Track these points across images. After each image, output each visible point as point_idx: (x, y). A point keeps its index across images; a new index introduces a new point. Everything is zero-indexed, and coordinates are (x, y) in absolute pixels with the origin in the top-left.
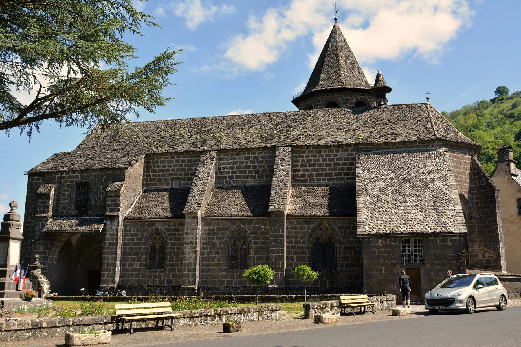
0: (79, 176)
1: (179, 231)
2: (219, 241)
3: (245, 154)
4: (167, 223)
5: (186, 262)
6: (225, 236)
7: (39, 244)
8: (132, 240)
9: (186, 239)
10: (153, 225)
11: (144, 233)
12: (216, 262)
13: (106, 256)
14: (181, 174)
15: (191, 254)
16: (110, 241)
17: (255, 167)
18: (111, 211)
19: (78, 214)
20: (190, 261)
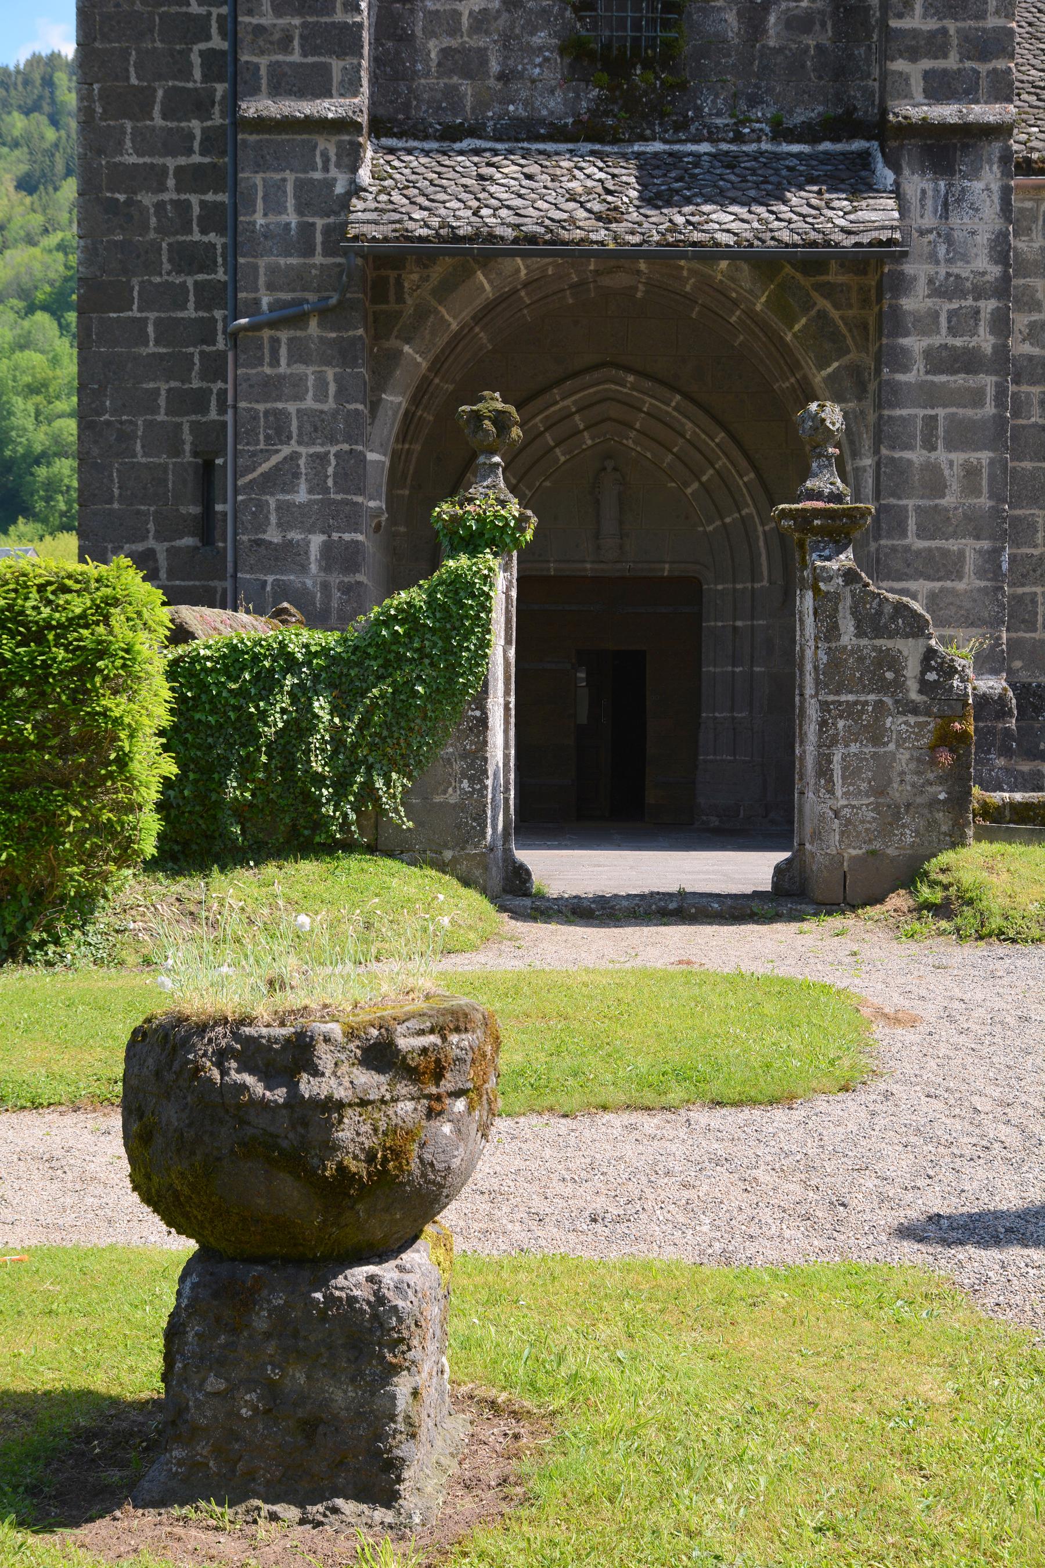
7: (299, 353)
13: (916, 456)
19: (593, 112)
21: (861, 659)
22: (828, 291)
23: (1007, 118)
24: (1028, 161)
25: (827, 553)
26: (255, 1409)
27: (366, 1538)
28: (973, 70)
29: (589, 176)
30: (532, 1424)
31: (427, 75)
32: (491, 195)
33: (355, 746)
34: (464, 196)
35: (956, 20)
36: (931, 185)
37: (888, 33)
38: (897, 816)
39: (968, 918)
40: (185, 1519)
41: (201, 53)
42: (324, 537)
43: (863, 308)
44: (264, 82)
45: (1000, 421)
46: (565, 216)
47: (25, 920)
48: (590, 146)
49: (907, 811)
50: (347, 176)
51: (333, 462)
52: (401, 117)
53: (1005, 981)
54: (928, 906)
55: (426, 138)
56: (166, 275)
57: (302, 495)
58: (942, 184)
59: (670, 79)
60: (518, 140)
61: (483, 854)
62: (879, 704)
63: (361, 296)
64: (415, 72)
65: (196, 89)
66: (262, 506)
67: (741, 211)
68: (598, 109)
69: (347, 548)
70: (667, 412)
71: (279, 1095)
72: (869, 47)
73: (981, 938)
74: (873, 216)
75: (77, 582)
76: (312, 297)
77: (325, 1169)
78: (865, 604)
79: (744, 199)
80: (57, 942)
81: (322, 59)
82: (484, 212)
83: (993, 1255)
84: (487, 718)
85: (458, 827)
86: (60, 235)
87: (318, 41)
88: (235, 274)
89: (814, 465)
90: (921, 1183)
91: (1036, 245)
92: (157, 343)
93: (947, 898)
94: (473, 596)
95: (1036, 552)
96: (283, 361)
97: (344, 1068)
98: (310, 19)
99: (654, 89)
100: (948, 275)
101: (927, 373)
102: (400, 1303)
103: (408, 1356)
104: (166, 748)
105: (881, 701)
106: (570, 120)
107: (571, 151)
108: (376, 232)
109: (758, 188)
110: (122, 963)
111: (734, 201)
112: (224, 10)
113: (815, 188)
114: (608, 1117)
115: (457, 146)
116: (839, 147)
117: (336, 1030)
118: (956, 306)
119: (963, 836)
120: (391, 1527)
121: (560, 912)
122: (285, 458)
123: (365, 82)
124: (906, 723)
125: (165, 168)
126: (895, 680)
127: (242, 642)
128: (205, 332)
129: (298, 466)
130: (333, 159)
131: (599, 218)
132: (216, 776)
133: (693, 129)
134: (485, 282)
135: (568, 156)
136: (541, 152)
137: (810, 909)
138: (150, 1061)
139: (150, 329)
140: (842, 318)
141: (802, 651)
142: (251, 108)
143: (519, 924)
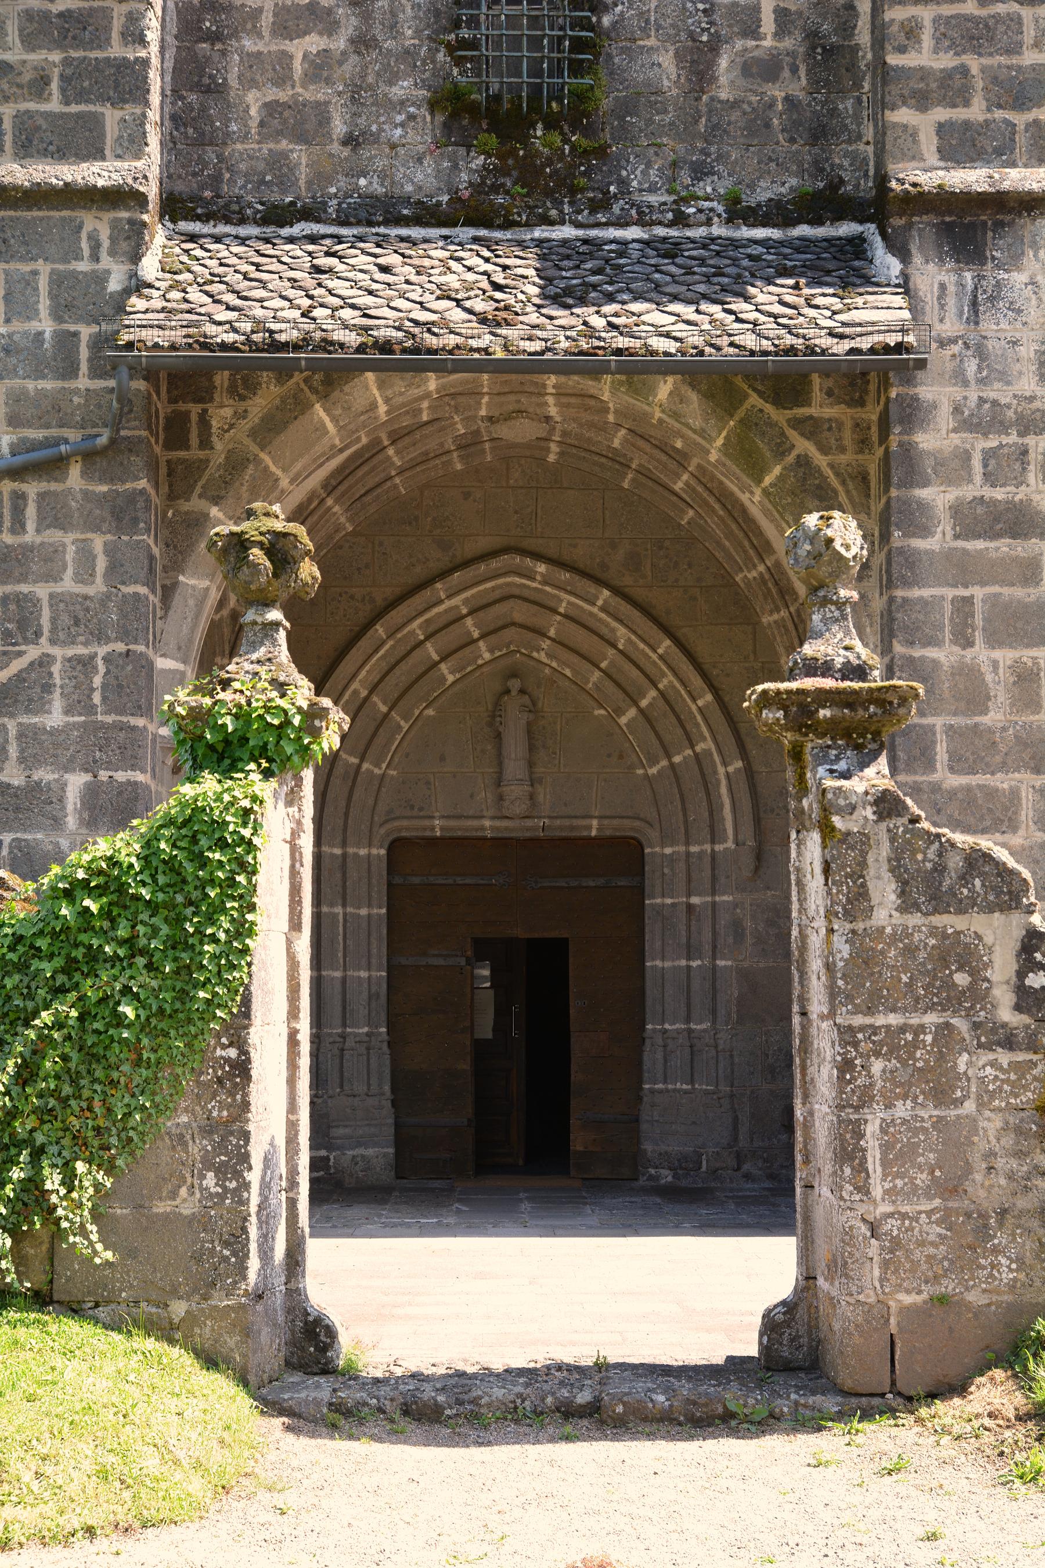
16: (975, 488)
21: (910, 951)
22: (810, 428)
25: (842, 766)
28: (1006, 122)
29: (470, 269)
31: (245, 137)
32: (330, 291)
34: (291, 293)
35: (980, 55)
36: (953, 278)
37: (881, 70)
38: (983, 1232)
42: (87, 777)
43: (861, 451)
44: (8, 139)
46: (434, 317)
48: (472, 232)
49: (1001, 1224)
50: (128, 267)
51: (102, 668)
52: (208, 194)
55: (242, 221)
57: (55, 717)
58: (968, 276)
59: (584, 143)
60: (370, 224)
61: (242, 1307)
63: (144, 433)
64: (228, 134)
67: (687, 311)
68: (483, 183)
69: (120, 793)
70: (591, 614)
72: (859, 101)
76: (73, 435)
78: (914, 853)
79: (689, 295)
81: (91, 108)
82: (318, 312)
84: (249, 1060)
85: (197, 1258)
87: (86, 84)
89: (816, 617)
94: (222, 844)
96: (31, 526)
98: (74, 54)
99: (562, 157)
100: (982, 400)
101: (956, 537)
105: (947, 1025)
106: (445, 198)
107: (446, 238)
109: (709, 282)
111: (675, 298)
113: (791, 282)
115: (286, 231)
118: (995, 444)
121: (381, 1410)
122: (32, 664)
124: (993, 1064)
126: (972, 987)
129: (50, 674)
130: (106, 243)
131: (483, 320)
133: (616, 209)
134: (327, 420)
135: (441, 244)
136: (402, 239)
137: (831, 1404)
140: (831, 466)
143: (304, 1441)
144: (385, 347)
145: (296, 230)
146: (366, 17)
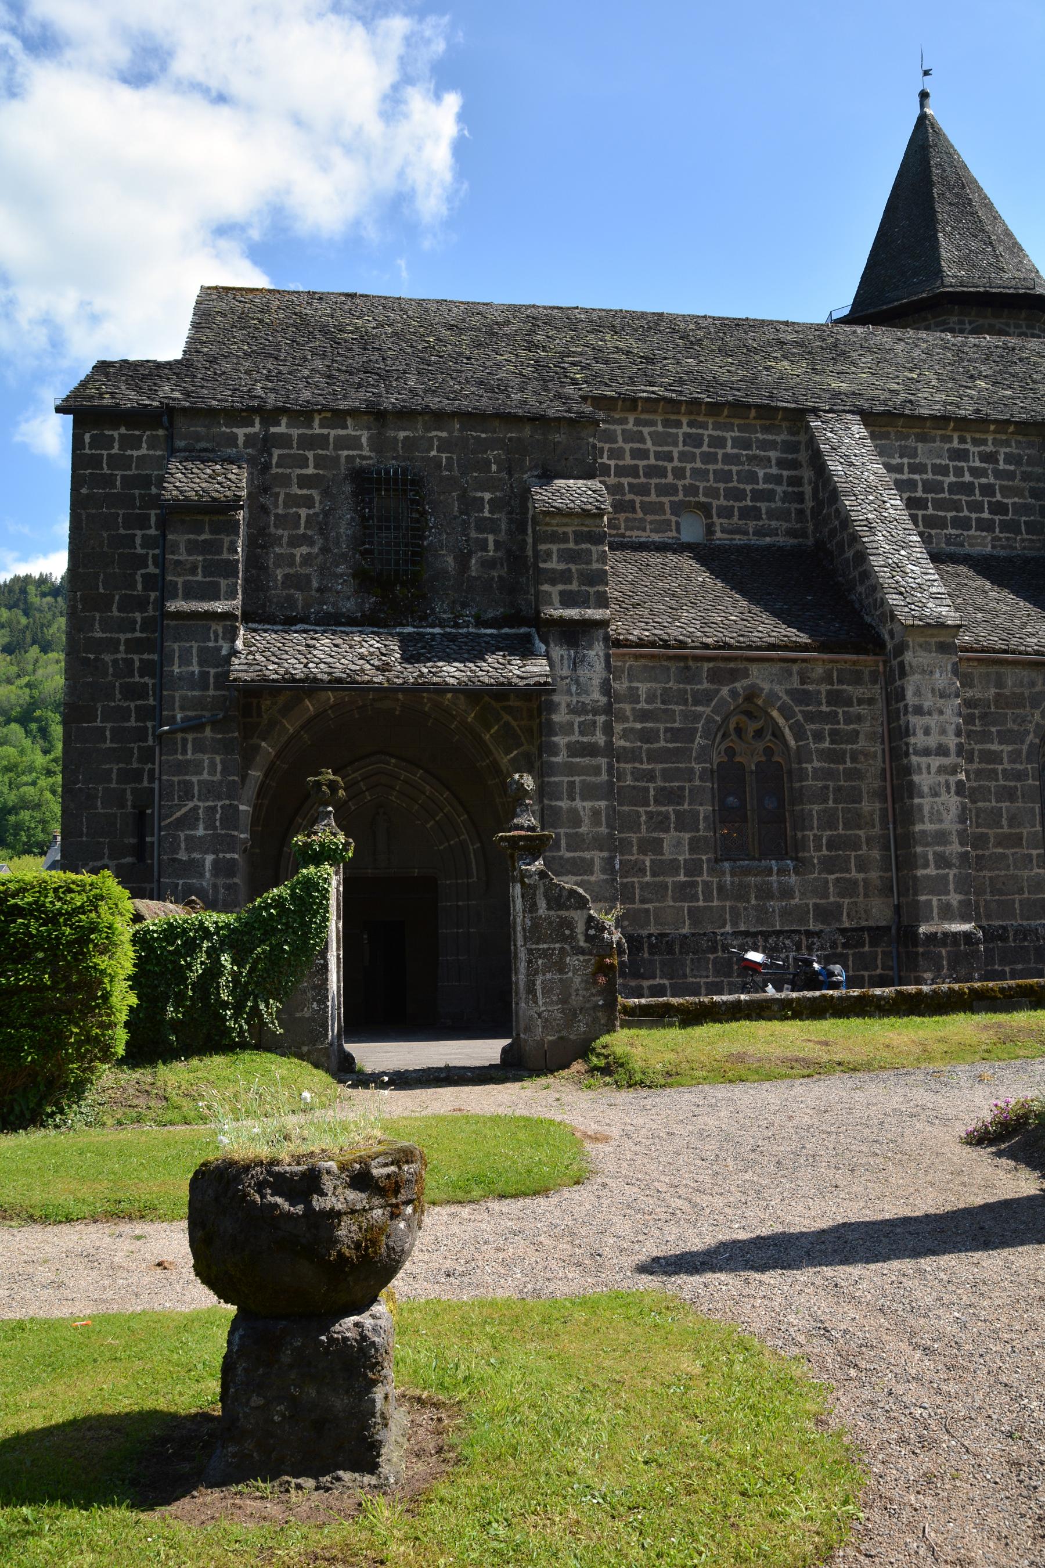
0: (364, 440)
1: (850, 704)
2: (1010, 748)
3: (950, 439)
4: (795, 668)
5: (929, 827)
6: (1031, 727)
7: (199, 748)
8: (647, 736)
9: (920, 732)
10: (734, 675)
11: (699, 709)
12: (1006, 830)
13: (564, 804)
14: (712, 493)
15: (944, 797)
17: (988, 490)
18: (569, 600)
20: (943, 826)
21: (550, 923)
22: (509, 710)
23: (606, 617)
24: (618, 640)
25: (528, 861)
26: (283, 1416)
27: (360, 1495)
30: (447, 1411)
31: (275, 589)
33: (247, 983)
37: (538, 571)
38: (575, 1015)
39: (621, 1074)
40: (240, 1493)
41: (142, 575)
42: (213, 857)
44: (180, 591)
45: (610, 783)
46: (358, 668)
47: (41, 1099)
48: (371, 629)
51: (220, 811)
53: (654, 1111)
54: (596, 1068)
55: (275, 623)
56: (118, 701)
57: (201, 832)
58: (572, 652)
60: (329, 625)
62: (562, 949)
64: (269, 587)
65: (138, 596)
66: (176, 838)
71: (299, 1209)
73: (630, 1086)
74: (535, 669)
75: (78, 886)
76: (207, 714)
77: (330, 1256)
80: (62, 1112)
82: (311, 665)
83: (696, 1279)
86: (27, 678)
88: (161, 701)
90: (641, 1238)
91: (624, 686)
92: (112, 741)
93: (608, 1063)
94: (318, 891)
95: (633, 858)
96: (189, 752)
97: (340, 1190)
101: (568, 756)
102: (377, 1339)
103: (382, 1373)
104: (131, 988)
108: (246, 677)
110: (104, 1124)
111: (456, 660)
112: (157, 551)
114: (437, 1209)
115: (293, 628)
116: (513, 631)
117: (332, 1165)
119: (614, 1026)
120: (375, 1487)
123: (240, 592)
124: (578, 960)
125: (119, 640)
126: (571, 934)
127: (176, 920)
128: (141, 734)
130: (221, 635)
131: (378, 668)
132: (160, 1004)
133: (430, 620)
136: (342, 632)
137: (526, 1073)
138: (210, 1191)
139: (108, 733)
140: (518, 726)
141: (515, 919)
142: (172, 606)
144: (339, 680)
145: (297, 627)
146: (326, 539)
